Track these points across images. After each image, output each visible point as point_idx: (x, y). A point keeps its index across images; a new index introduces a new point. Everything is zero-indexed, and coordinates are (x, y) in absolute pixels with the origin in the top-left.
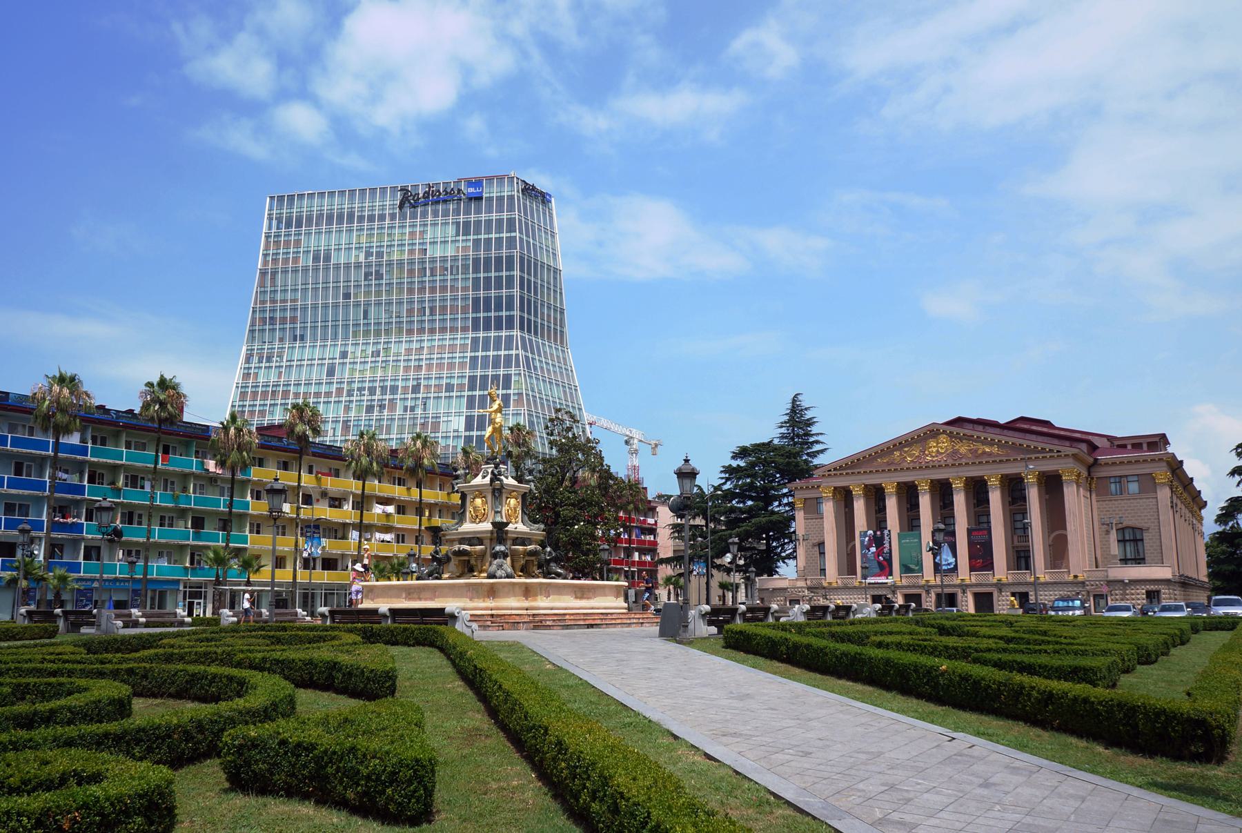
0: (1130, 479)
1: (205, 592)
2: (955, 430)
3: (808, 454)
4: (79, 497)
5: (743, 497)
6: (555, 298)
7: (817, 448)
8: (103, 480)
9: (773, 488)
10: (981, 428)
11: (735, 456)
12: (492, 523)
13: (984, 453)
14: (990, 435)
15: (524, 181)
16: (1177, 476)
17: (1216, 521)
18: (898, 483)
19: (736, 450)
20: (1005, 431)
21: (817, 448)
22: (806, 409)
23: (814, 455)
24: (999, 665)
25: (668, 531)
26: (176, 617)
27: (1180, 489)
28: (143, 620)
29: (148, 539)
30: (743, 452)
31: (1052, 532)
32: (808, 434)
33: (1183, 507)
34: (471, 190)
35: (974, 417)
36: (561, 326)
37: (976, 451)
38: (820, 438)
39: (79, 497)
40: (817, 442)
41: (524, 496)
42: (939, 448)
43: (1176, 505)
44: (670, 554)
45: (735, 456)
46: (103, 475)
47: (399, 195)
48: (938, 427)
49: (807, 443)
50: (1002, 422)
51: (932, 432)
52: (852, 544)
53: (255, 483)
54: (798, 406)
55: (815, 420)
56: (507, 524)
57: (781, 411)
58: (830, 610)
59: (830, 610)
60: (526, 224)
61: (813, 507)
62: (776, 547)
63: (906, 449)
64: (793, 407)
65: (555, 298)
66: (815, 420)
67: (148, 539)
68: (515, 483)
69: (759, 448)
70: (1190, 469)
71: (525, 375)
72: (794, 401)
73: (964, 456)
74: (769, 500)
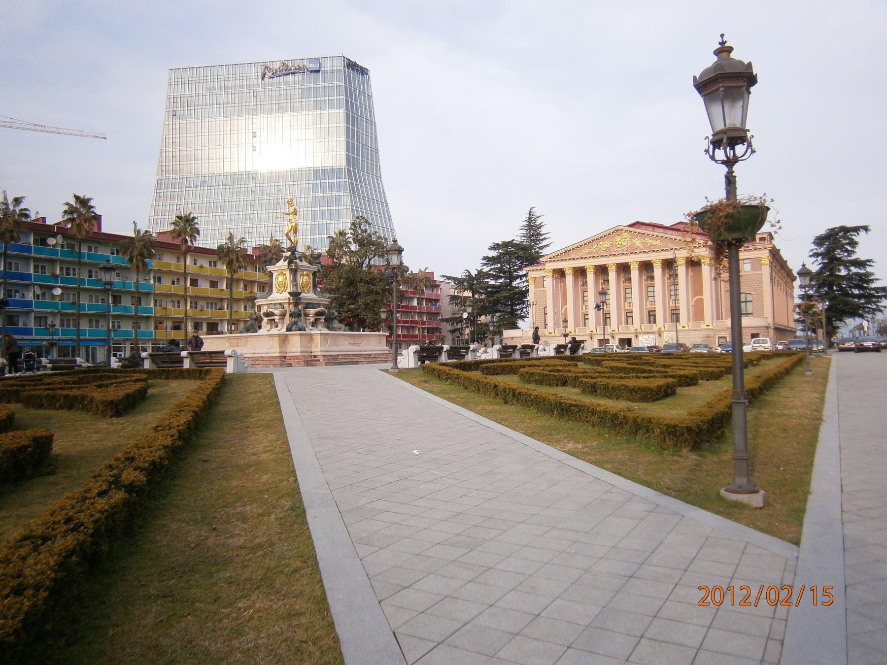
0: (746, 261)
1: (125, 347)
2: (633, 229)
3: (539, 248)
4: (27, 282)
5: (496, 277)
6: (371, 142)
7: (544, 243)
8: (45, 270)
9: (515, 271)
10: (651, 228)
11: (492, 248)
12: (289, 293)
13: (652, 245)
14: (659, 233)
15: (348, 59)
16: (777, 259)
17: (814, 243)
18: (595, 266)
19: (492, 245)
20: (667, 231)
21: (544, 243)
22: (538, 217)
23: (542, 248)
24: (705, 367)
25: (448, 300)
26: (76, 363)
27: (779, 268)
28: (50, 365)
29: (79, 311)
30: (495, 247)
31: (695, 296)
32: (539, 234)
33: (780, 279)
34: (312, 65)
35: (648, 221)
36: (376, 162)
37: (647, 244)
38: (547, 236)
39: (27, 282)
40: (544, 239)
41: (314, 274)
42: (624, 240)
43: (775, 278)
44: (450, 316)
45: (492, 248)
46: (45, 267)
47: (261, 70)
48: (622, 228)
49: (539, 240)
50: (668, 224)
51: (617, 231)
52: (565, 307)
53: (155, 271)
54: (533, 215)
55: (543, 224)
56: (300, 293)
57: (522, 220)
58: (518, 348)
59: (518, 348)
60: (351, 90)
61: (539, 282)
62: (517, 310)
63: (601, 243)
64: (530, 216)
65: (371, 142)
66: (543, 224)
67: (79, 311)
68: (308, 265)
69: (506, 245)
70: (784, 255)
71: (351, 196)
72: (530, 212)
73: (638, 248)
74: (513, 279)
